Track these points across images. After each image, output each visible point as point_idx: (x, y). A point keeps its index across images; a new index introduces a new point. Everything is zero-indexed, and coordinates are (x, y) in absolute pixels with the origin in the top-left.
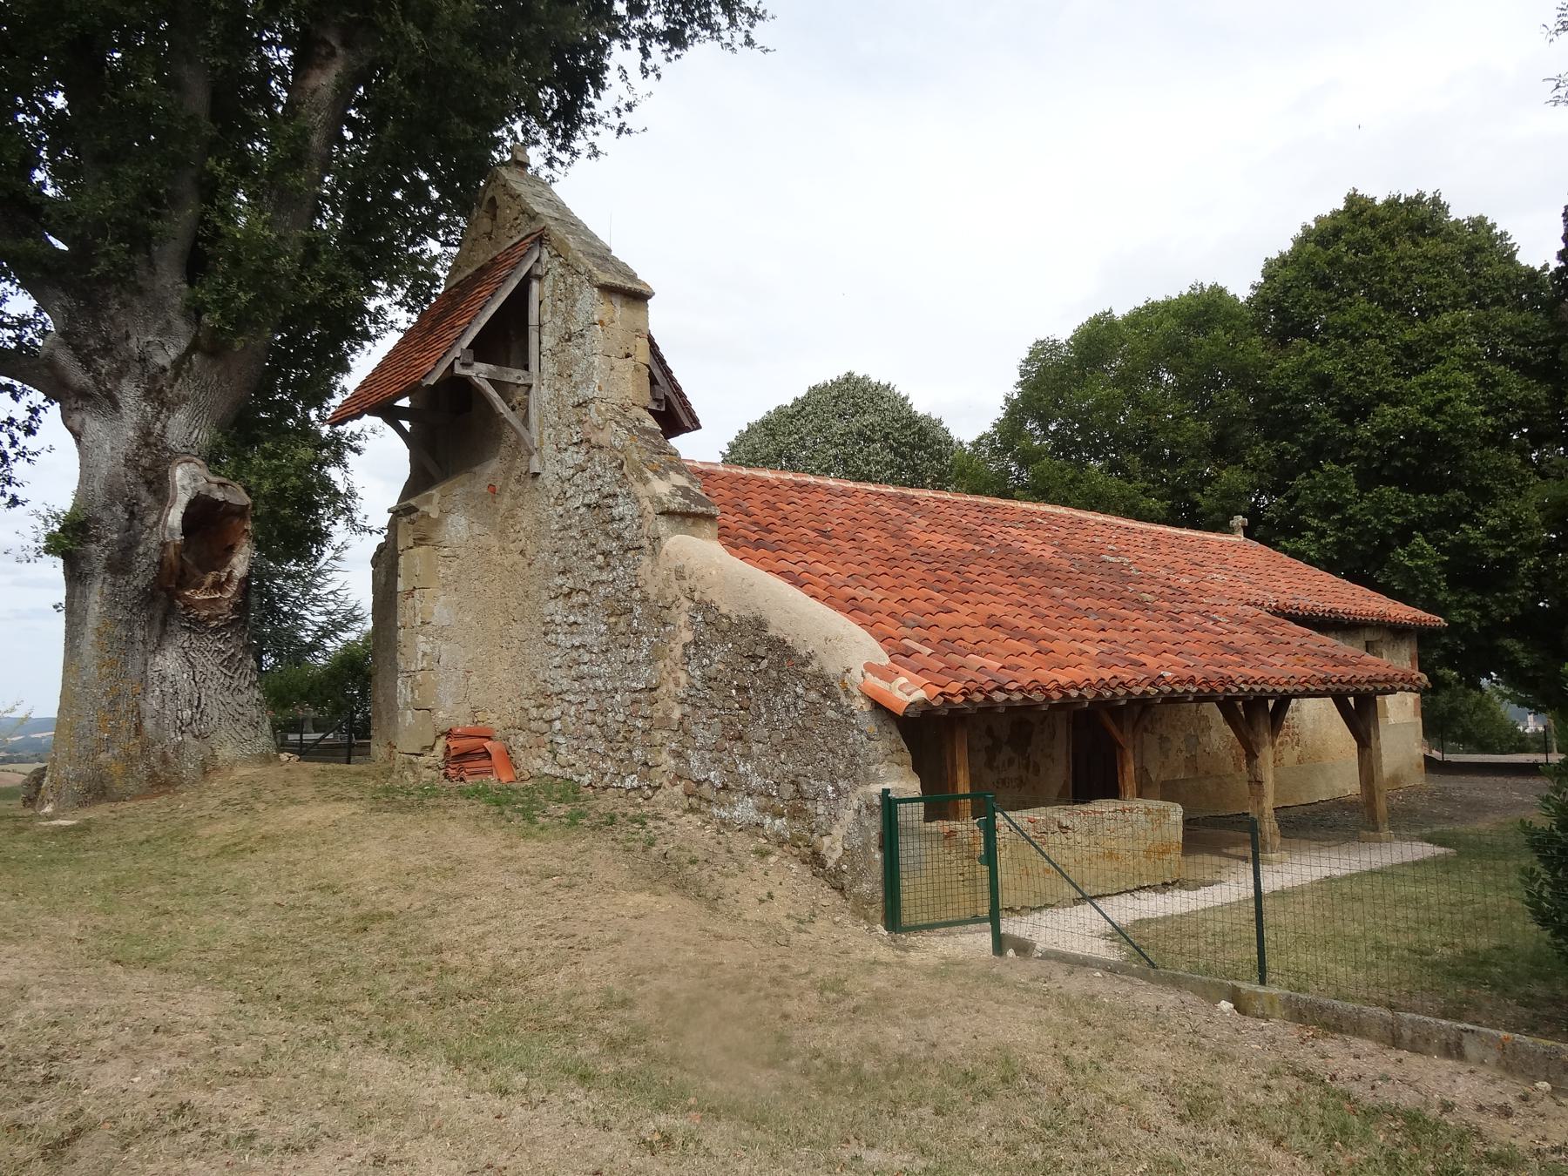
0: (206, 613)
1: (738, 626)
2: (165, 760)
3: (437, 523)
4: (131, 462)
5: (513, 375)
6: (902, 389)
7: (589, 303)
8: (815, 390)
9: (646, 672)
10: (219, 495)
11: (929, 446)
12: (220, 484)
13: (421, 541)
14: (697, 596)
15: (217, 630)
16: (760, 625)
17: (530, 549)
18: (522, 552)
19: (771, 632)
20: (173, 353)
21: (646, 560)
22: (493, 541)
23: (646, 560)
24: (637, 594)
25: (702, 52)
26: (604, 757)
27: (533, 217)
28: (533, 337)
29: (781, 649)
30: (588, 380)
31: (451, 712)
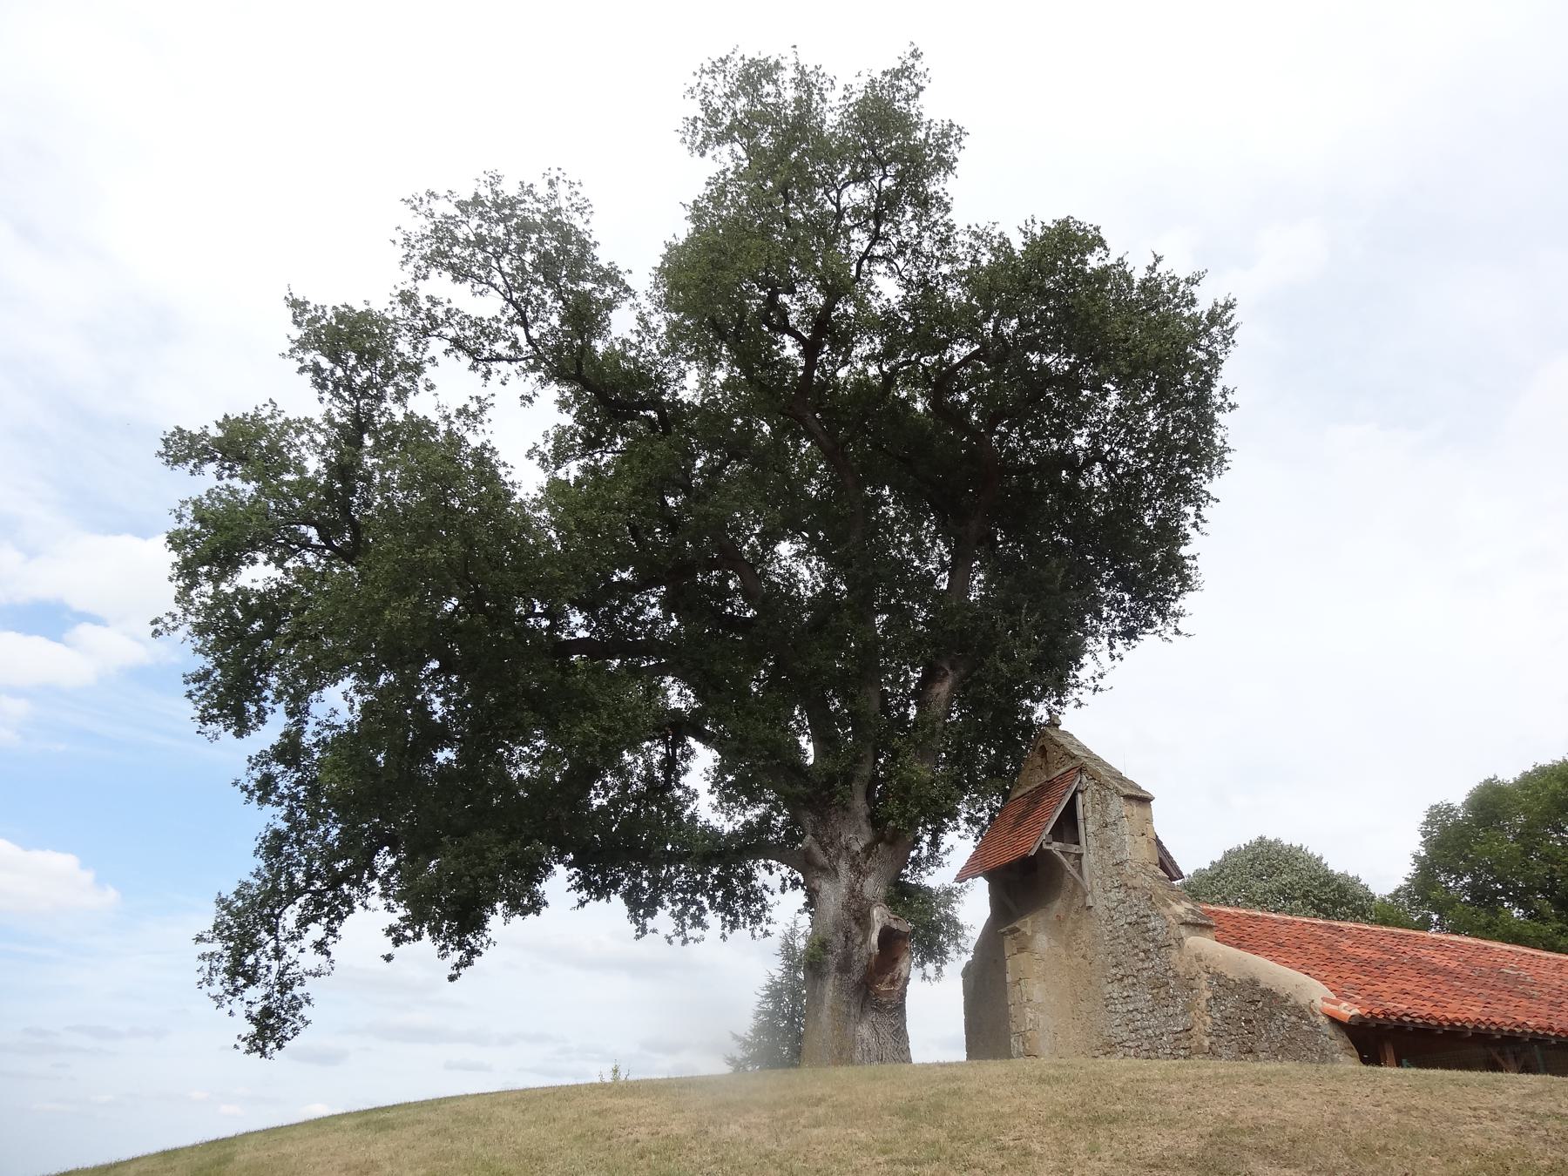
1: (1240, 985)
3: (1032, 937)
4: (846, 907)
5: (1074, 848)
6: (1314, 849)
7: (1117, 805)
8: (1229, 854)
9: (1182, 1020)
10: (895, 926)
11: (1350, 902)
13: (1021, 950)
16: (1254, 983)
17: (1090, 954)
18: (1084, 957)
19: (1262, 986)
20: (862, 844)
21: (1175, 952)
22: (1062, 951)
23: (1175, 952)
24: (1170, 973)
25: (1148, 642)
27: (1074, 757)
28: (1081, 826)
29: (1269, 993)
30: (1123, 850)
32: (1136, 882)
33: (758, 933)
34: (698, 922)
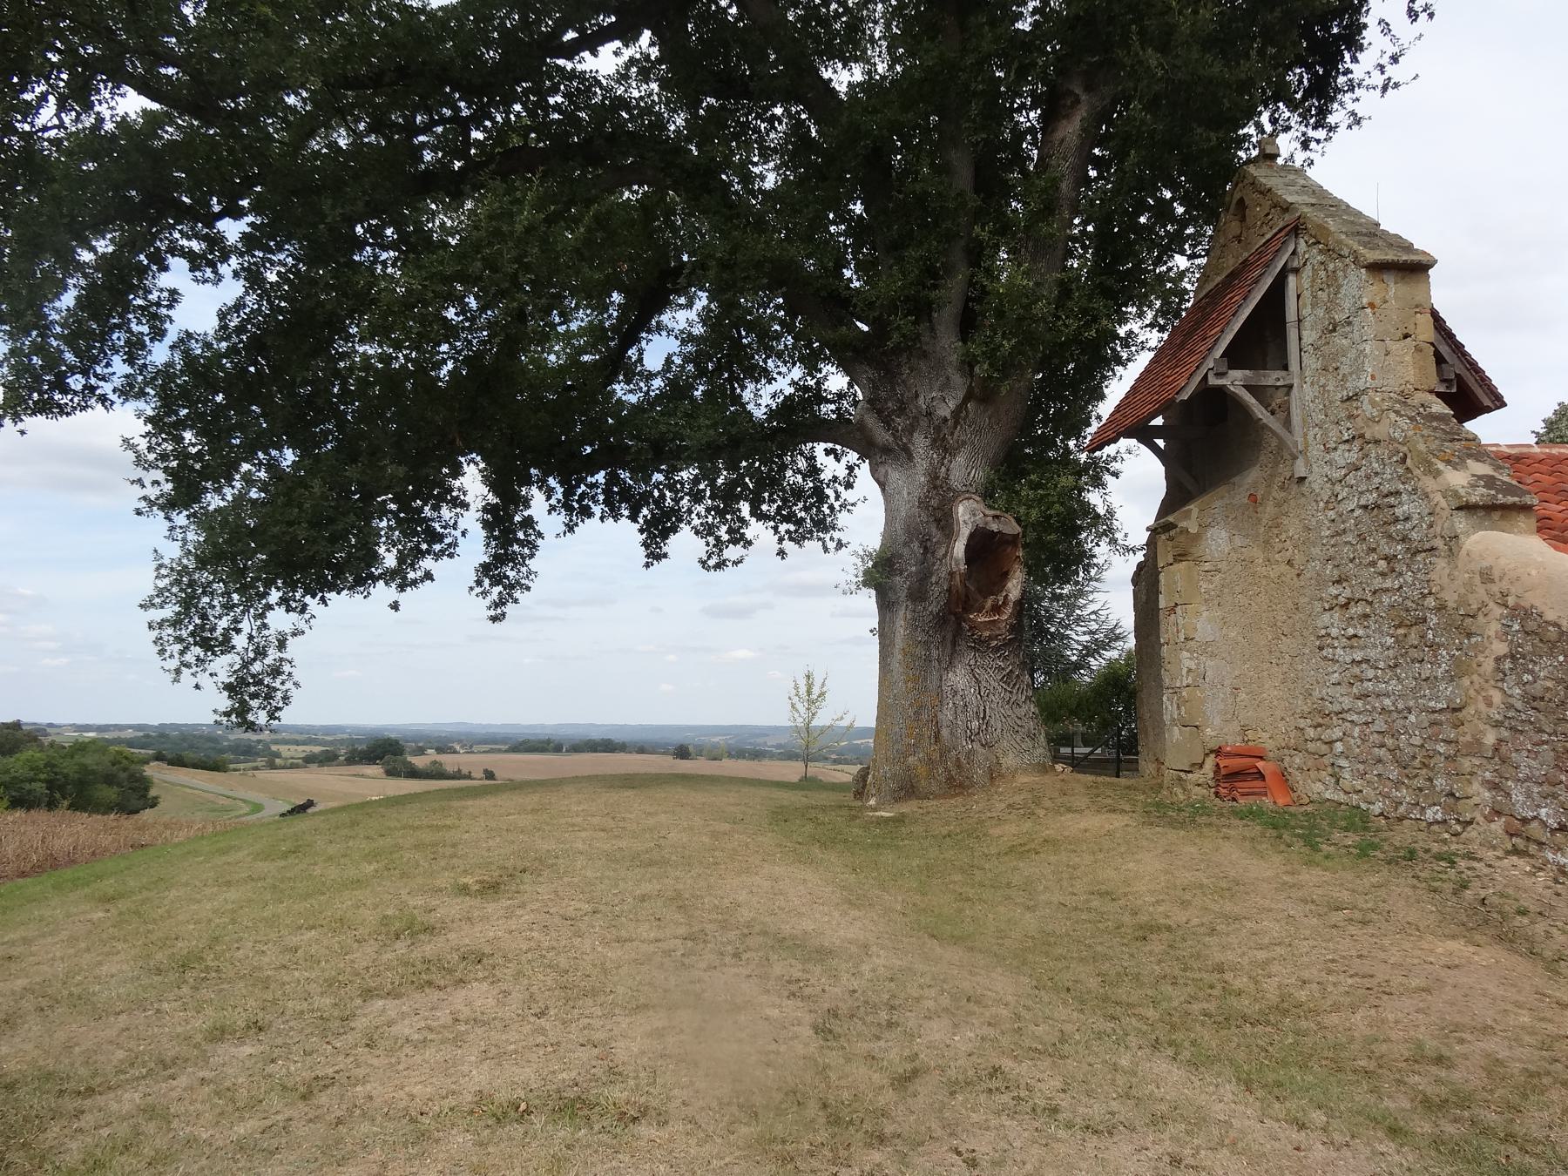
0: (987, 633)
2: (959, 765)
3: (1197, 537)
4: (923, 504)
5: (1272, 378)
7: (1356, 286)
9: (1446, 689)
10: (994, 527)
12: (996, 517)
14: (1511, 601)
15: (997, 649)
17: (1299, 559)
20: (952, 404)
21: (1441, 563)
22: (1257, 553)
23: (1441, 563)
24: (1430, 602)
26: (1398, 784)
27: (1287, 208)
30: (1358, 371)
31: (1219, 729)
32: (1379, 431)
33: (831, 545)
34: (737, 538)
